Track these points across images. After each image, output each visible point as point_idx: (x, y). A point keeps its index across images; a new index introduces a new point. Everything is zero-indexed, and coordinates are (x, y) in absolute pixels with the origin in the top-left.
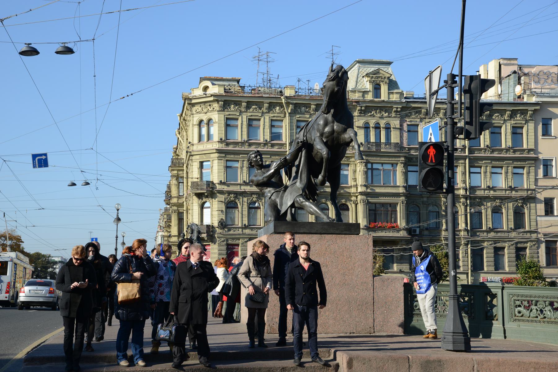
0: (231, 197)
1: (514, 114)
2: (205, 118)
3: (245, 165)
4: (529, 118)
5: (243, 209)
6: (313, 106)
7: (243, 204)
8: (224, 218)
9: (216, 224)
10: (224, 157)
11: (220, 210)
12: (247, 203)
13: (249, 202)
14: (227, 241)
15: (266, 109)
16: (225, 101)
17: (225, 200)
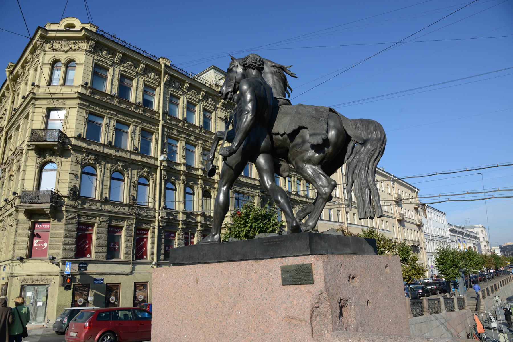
0: (91, 159)
1: (172, 81)
2: (63, 58)
3: (112, 124)
4: (141, 72)
5: (105, 178)
6: (187, 84)
7: (104, 172)
8: (78, 186)
9: (64, 191)
10: (88, 107)
11: (73, 174)
12: (111, 171)
13: (112, 170)
14: (79, 217)
15: (142, 70)
16: (98, 43)
17: (82, 162)
